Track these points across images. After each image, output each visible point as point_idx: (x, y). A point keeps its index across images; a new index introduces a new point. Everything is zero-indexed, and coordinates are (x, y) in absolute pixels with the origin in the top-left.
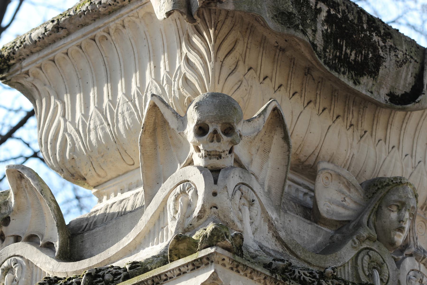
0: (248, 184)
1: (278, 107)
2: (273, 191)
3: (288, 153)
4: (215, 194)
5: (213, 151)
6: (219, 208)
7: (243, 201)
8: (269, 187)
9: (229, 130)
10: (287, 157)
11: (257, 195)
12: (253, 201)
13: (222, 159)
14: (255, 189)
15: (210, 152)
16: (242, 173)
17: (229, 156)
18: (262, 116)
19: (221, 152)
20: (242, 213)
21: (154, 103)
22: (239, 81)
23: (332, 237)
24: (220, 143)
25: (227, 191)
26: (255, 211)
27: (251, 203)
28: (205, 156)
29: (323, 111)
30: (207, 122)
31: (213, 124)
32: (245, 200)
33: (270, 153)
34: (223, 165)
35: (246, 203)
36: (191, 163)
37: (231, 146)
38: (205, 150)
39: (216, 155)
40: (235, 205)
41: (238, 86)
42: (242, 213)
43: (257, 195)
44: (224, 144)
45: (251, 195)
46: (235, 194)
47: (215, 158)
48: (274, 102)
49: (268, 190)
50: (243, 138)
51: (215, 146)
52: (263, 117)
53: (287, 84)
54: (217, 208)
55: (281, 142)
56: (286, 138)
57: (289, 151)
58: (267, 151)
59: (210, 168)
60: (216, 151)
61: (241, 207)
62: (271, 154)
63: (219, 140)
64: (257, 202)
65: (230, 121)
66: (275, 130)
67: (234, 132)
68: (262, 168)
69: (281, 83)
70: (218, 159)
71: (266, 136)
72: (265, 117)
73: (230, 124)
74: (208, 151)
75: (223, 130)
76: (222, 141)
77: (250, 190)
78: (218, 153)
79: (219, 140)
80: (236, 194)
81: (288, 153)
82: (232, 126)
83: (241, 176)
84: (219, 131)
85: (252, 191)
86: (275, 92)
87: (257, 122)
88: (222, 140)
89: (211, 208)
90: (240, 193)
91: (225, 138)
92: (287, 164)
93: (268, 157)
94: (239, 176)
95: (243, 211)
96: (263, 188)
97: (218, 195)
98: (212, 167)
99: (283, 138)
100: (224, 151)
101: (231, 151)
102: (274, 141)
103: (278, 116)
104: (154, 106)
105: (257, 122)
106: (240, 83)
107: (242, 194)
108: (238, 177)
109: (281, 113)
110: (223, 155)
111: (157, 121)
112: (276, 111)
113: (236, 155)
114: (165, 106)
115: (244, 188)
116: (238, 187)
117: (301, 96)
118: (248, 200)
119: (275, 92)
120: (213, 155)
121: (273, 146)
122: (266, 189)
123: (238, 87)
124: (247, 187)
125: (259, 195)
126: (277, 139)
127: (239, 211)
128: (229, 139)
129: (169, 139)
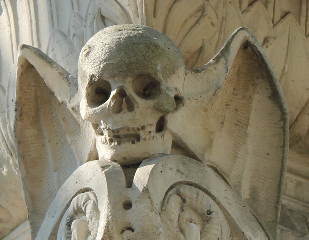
0: (197, 183)
1: (250, 39)
2: (262, 196)
3: (282, 122)
4: (128, 205)
5: (123, 128)
6: (137, 229)
7: (188, 214)
8: (254, 192)
9: (150, 88)
10: (282, 131)
11: (218, 203)
12: (209, 213)
13: (142, 141)
14: (213, 193)
15: (118, 130)
16: (184, 164)
17: (159, 135)
18: (222, 60)
19: (138, 129)
20: (184, 235)
21: (27, 61)
22: (198, 11)
23: (257, 228)
24: (133, 113)
25: (150, 198)
26: (215, 232)
27: (206, 217)
28: (111, 141)
29: (283, 17)
30: (106, 77)
31: (117, 79)
32: (192, 212)
33: (249, 128)
34: (145, 153)
35: (194, 217)
36: (94, 156)
37: (158, 116)
38: (109, 129)
39: (131, 135)
40: (169, 222)
41: (196, 19)
42: (184, 235)
43: (218, 203)
44: (144, 112)
45: (205, 202)
46: (168, 203)
47: (129, 141)
48: (241, 31)
49: (251, 195)
50: (187, 102)
51: (125, 119)
52: (225, 62)
53: (300, 11)
54: (133, 230)
55: (269, 105)
56: (275, 96)
57: (283, 119)
58: (242, 125)
59: (123, 161)
60: (128, 129)
61: (183, 226)
62: (250, 130)
63: (131, 107)
64: (218, 217)
65: (150, 71)
66: (254, 84)
67: (160, 90)
68: (235, 157)
69: (286, 9)
70: (133, 143)
71: (238, 97)
72: (227, 61)
73: (149, 76)
74: (113, 131)
75: (141, 91)
76: (136, 109)
77: (201, 192)
78: (131, 132)
79: (131, 107)
80: (170, 201)
81: (282, 122)
82: (154, 79)
83: (182, 169)
84: (130, 91)
85: (206, 196)
86: (274, 25)
87: (214, 71)
88: (136, 106)
89: (123, 231)
90: (179, 199)
91: (141, 103)
92: (282, 144)
93: (246, 135)
94: (178, 170)
95: (186, 233)
96: (239, 193)
97: (134, 206)
98: (125, 159)
99: (270, 98)
100: (143, 128)
101: (161, 126)
102: (255, 104)
103: (255, 58)
104: (27, 68)
105: (214, 71)
106: (199, 14)
107: (184, 201)
108: (175, 171)
109: (258, 52)
110: (142, 134)
111: (39, 94)
112: (249, 49)
113: (174, 135)
114: (45, 63)
115: (187, 191)
116: (174, 189)
117: (299, 21)
118: (199, 211)
119: (274, 25)
120: (126, 136)
121: (253, 115)
122: (245, 193)
123: (197, 22)
124: (194, 189)
125: (224, 203)
126: (259, 100)
127: (180, 234)
128: (151, 103)
129: (62, 122)
